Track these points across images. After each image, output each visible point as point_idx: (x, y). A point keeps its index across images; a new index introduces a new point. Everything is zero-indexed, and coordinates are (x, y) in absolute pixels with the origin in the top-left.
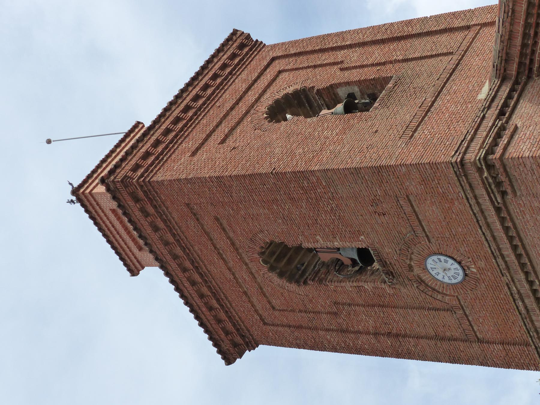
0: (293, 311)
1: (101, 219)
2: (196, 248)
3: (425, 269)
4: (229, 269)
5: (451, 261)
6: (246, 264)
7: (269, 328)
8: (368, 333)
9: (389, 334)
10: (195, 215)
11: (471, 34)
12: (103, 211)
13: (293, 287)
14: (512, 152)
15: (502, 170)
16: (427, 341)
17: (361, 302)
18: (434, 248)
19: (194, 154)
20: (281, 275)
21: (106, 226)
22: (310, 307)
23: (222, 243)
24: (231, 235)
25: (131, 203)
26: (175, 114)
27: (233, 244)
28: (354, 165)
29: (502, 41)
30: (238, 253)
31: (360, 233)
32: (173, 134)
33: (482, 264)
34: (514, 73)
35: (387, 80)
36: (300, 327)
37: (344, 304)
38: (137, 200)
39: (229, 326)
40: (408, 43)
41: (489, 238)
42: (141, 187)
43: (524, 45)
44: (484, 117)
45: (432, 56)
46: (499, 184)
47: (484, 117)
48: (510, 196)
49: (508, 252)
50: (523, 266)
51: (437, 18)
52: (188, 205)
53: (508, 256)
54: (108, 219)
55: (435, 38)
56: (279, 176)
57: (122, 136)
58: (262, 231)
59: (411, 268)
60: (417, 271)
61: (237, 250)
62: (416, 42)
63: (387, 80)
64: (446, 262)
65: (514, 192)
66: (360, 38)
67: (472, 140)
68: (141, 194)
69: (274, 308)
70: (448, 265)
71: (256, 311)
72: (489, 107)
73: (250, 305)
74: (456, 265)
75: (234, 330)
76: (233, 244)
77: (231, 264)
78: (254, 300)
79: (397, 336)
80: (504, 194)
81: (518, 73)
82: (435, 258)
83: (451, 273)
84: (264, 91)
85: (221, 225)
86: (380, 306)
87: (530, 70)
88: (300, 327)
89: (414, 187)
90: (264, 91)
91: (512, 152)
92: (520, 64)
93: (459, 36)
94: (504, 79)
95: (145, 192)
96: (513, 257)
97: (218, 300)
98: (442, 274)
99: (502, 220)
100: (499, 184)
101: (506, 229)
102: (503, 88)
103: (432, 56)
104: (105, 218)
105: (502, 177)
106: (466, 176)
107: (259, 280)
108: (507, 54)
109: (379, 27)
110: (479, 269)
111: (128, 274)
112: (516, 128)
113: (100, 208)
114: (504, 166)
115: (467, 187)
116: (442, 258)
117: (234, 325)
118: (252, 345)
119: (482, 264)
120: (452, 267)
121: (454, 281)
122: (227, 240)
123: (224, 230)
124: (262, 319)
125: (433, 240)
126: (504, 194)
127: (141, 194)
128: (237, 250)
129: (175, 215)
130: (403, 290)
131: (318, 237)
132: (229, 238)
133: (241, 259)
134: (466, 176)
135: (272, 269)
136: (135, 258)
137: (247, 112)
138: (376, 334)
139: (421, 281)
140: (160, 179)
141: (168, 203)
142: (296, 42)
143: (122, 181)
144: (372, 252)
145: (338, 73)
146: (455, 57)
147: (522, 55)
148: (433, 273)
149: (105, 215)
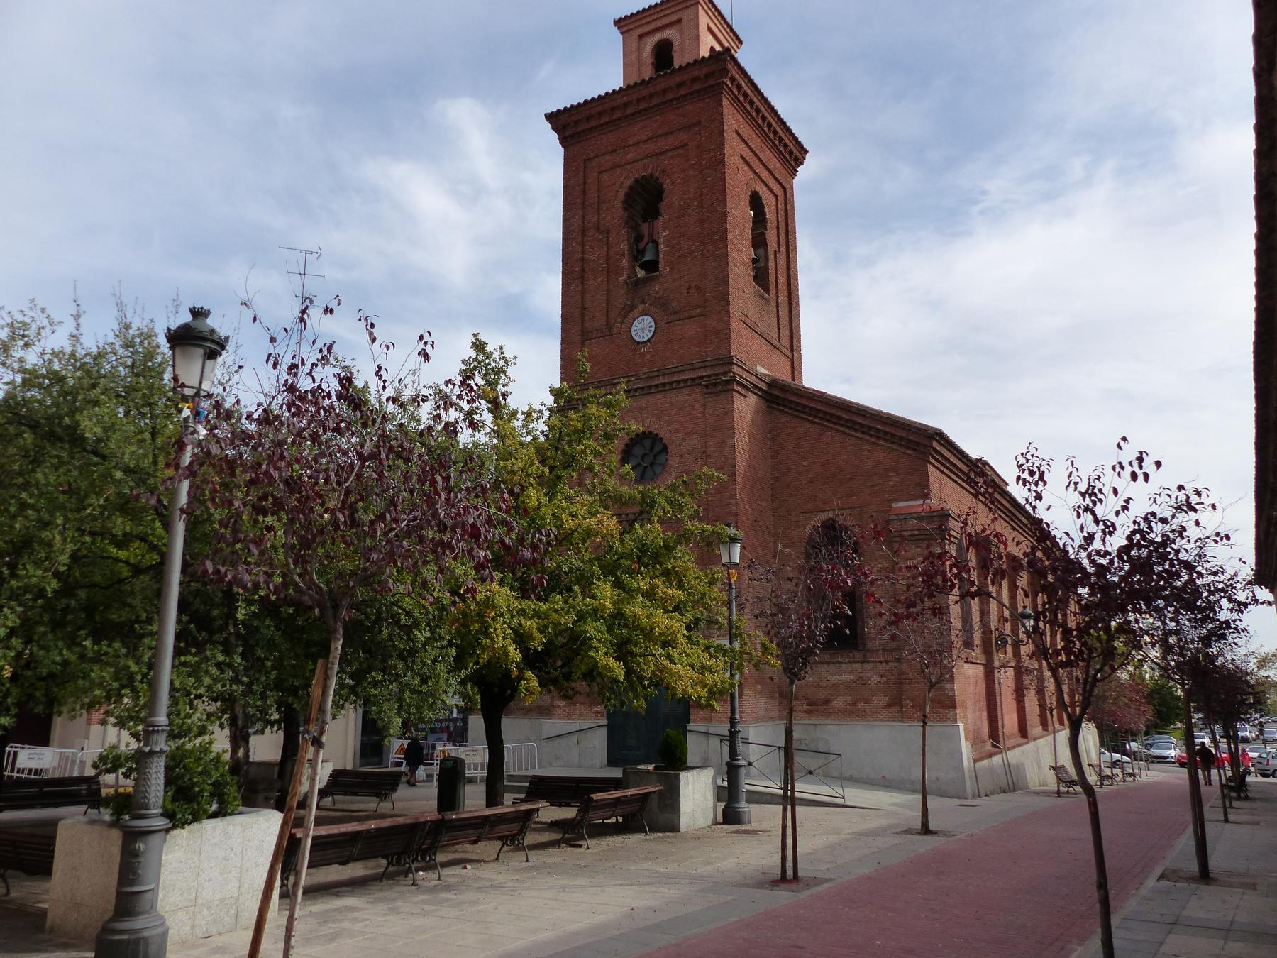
0: (599, 190)
1: (672, 6)
2: (658, 117)
3: (643, 314)
4: (638, 143)
5: (650, 335)
6: (641, 160)
7: (582, 165)
8: (583, 253)
9: (583, 270)
10: (690, 126)
11: (788, 353)
12: (680, 10)
13: (621, 197)
14: (736, 396)
15: (725, 388)
16: (580, 301)
17: (611, 253)
18: (660, 324)
19: (737, 132)
20: (631, 188)
21: (666, 9)
22: (604, 207)
23: (662, 144)
24: (670, 154)
25: (705, 71)
26: (763, 110)
27: (662, 153)
28: (730, 280)
29: (797, 389)
30: (652, 156)
31: (672, 269)
32: (749, 108)
33: (648, 357)
34: (773, 392)
35: (767, 291)
36: (584, 193)
37: (608, 238)
38: (707, 76)
39: (582, 127)
40: (786, 304)
41: (674, 370)
42: (718, 84)
43: (791, 402)
44: (752, 374)
45: (778, 325)
46: (715, 385)
47: (752, 374)
48: (704, 390)
49: (661, 380)
50: (650, 387)
51: (799, 325)
52: (699, 123)
53: (658, 379)
54: (673, 13)
55: (788, 325)
56: (724, 216)
57: (729, 20)
58: (673, 182)
59: (643, 302)
60: (641, 307)
61: (656, 155)
62: (787, 311)
63: (767, 291)
64: (650, 331)
65: (708, 393)
66: (792, 262)
67: (742, 368)
68: (712, 82)
69: (601, 172)
70: (646, 332)
71: (598, 156)
72: (757, 377)
73: (603, 152)
74: (646, 338)
75: (579, 129)
76: (662, 153)
77: (643, 146)
78: (608, 157)
79: (582, 277)
80: (707, 387)
81: (772, 394)
82: (653, 324)
83: (640, 333)
84: (767, 185)
85: (680, 148)
86: (608, 268)
87: (773, 402)
88: (584, 193)
89: (712, 322)
90: (767, 185)
91: (736, 396)
92: (778, 397)
93: (787, 344)
94: (769, 385)
95: (712, 86)
96: (656, 383)
97: (606, 123)
98: (640, 326)
99: (685, 381)
100: (715, 385)
101: (678, 382)
102: (765, 385)
103: (778, 325)
104: (673, 10)
105: (720, 388)
106: (722, 364)
107: (628, 167)
108: (787, 391)
109: (797, 280)
110: (644, 353)
111: (617, 17)
112: (745, 397)
113: (683, 8)
114: (728, 390)
115: (713, 363)
116: (653, 329)
117: (584, 131)
118: (564, 141)
119: (648, 357)
120: (645, 336)
121: (633, 334)
122: (1048, 626)
123: (675, 149)
124: (590, 159)
125: (667, 325)
126: (707, 387)
127: (712, 82)
128: (656, 155)
129: (690, 107)
130: (622, 291)
131: (668, 233)
132: (667, 151)
133: (647, 157)
134: (722, 364)
135: (637, 181)
136: (632, 29)
137: (756, 173)
138: (583, 260)
139: (632, 308)
140: (724, 103)
141: (701, 105)
142: (793, 207)
143: (726, 68)
144: (655, 274)
145: (773, 249)
146: (777, 344)
147: (784, 399)
148: (639, 319)
149: (676, 11)
